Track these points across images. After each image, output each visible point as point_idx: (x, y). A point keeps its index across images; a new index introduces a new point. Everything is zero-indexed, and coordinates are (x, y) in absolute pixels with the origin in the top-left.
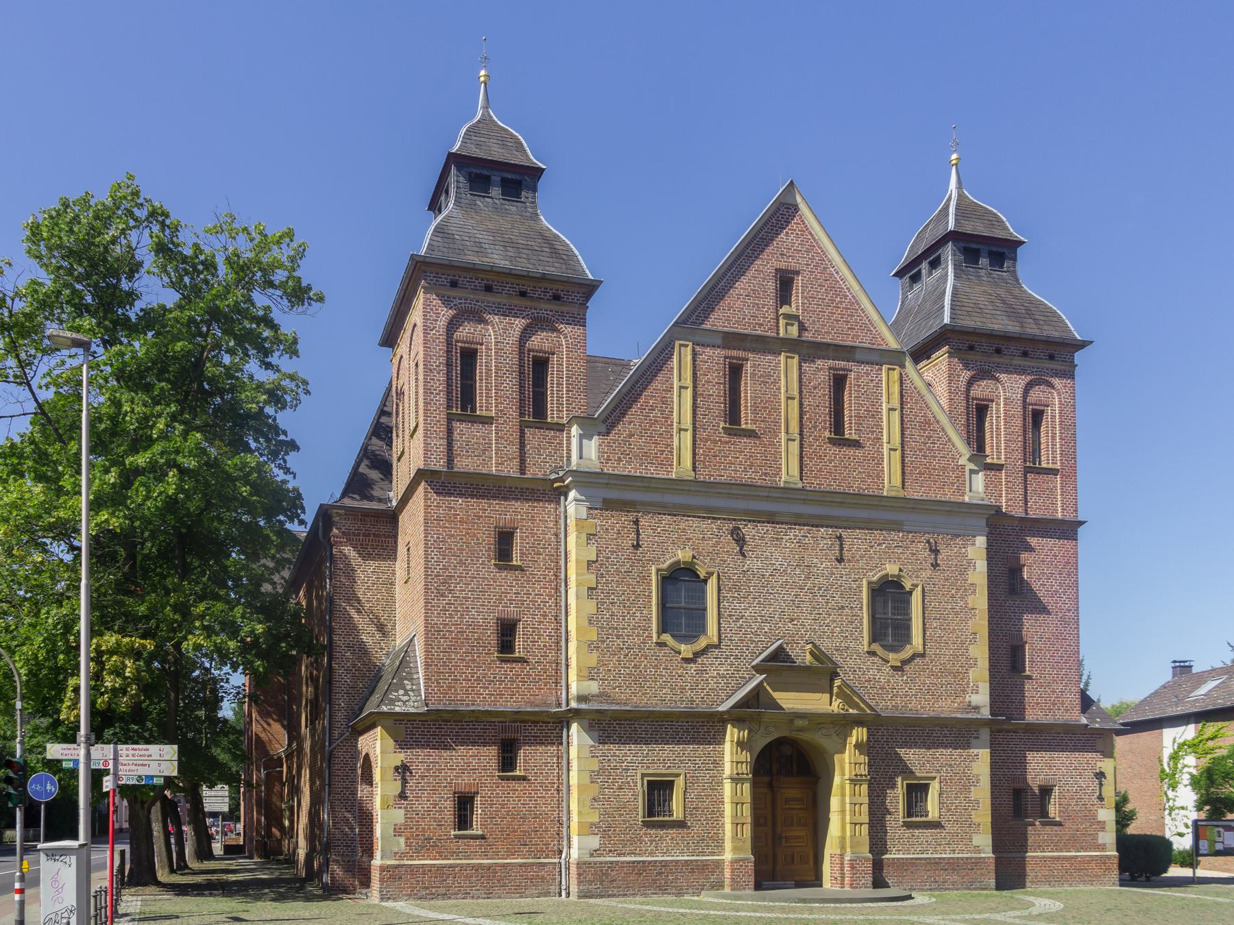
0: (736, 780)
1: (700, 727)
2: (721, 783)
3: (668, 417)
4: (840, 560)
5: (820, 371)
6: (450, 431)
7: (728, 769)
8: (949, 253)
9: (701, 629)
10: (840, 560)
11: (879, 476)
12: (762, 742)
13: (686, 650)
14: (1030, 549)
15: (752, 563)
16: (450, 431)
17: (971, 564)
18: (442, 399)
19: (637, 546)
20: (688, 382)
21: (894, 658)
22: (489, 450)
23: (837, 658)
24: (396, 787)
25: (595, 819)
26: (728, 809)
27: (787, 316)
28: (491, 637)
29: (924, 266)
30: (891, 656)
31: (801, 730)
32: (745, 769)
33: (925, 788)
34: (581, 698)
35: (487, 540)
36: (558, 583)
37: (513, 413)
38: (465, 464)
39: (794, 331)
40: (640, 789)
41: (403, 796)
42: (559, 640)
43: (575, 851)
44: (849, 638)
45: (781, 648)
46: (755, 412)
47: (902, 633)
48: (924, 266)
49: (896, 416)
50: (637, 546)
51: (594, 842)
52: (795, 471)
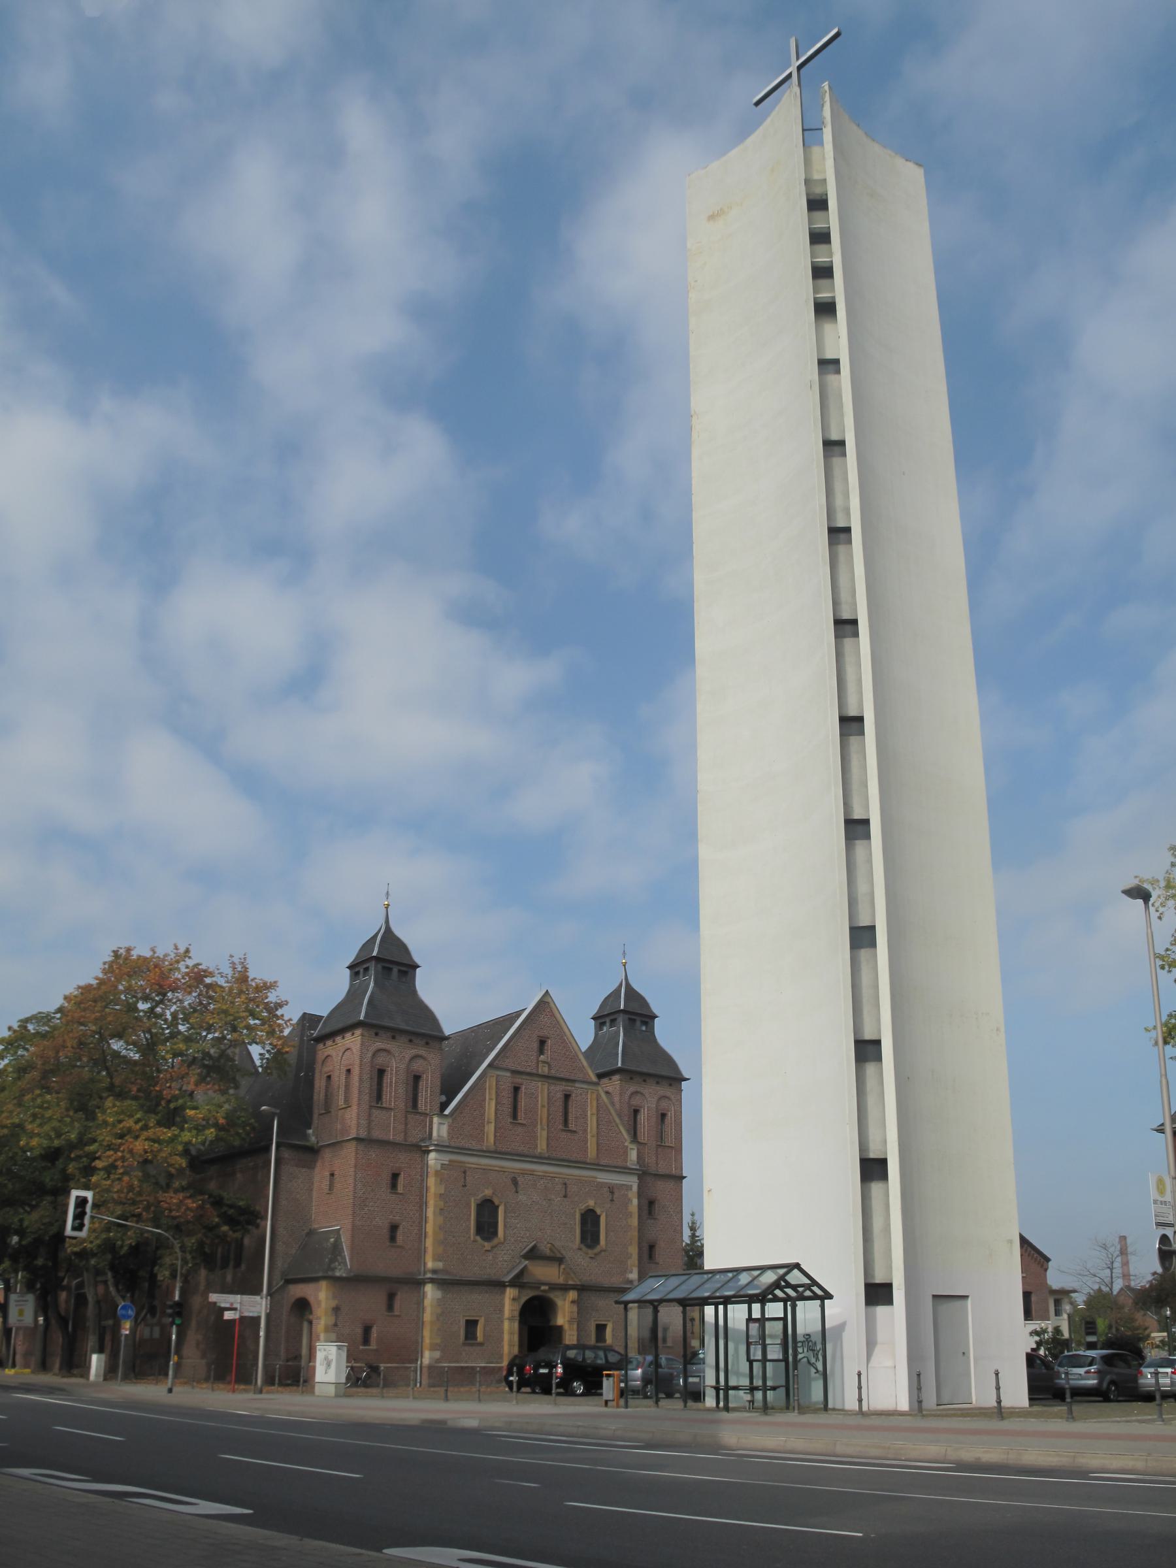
0: (511, 1319)
1: (500, 1285)
2: (502, 1322)
3: (483, 1115)
4: (565, 1196)
5: (559, 1090)
6: (370, 1115)
7: (507, 1313)
8: (621, 1020)
9: (495, 1233)
10: (565, 1196)
11: (586, 1151)
12: (524, 1300)
13: (487, 1246)
14: (97, 978)
15: (522, 1197)
16: (370, 1115)
17: (630, 1200)
18: (367, 1098)
19: (464, 1186)
20: (494, 1096)
21: (591, 1252)
22: (391, 1127)
23: (564, 1252)
24: (332, 1320)
25: (438, 1341)
26: (506, 1337)
27: (544, 1062)
28: (385, 1232)
29: (608, 1020)
30: (590, 1251)
31: (544, 1291)
32: (517, 1313)
33: (605, 1326)
34: (434, 1271)
35: (386, 1177)
36: (422, 1205)
37: (402, 1105)
38: (377, 1134)
39: (546, 1069)
40: (463, 1323)
41: (336, 1325)
42: (421, 1235)
43: (427, 1357)
44: (569, 1240)
45: (534, 1247)
46: (526, 1114)
47: (596, 1240)
48: (608, 1020)
49: (595, 1118)
50: (464, 1186)
51: (437, 1354)
52: (545, 1147)
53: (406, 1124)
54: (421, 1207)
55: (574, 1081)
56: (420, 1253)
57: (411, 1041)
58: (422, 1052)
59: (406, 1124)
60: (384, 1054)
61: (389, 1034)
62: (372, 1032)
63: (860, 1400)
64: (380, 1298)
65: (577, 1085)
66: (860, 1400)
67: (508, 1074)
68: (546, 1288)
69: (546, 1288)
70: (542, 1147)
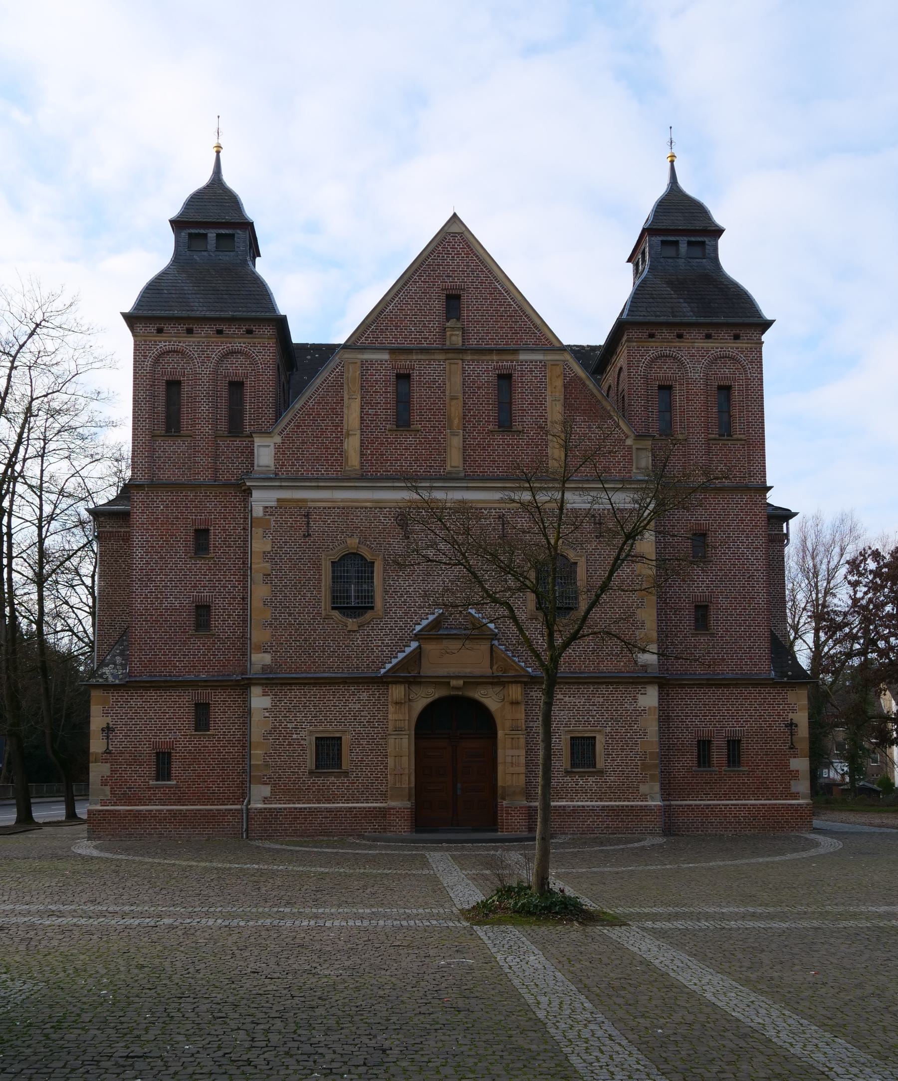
14: (452, 279)
53: (216, 457)
54: (245, 575)
55: (515, 351)
56: (243, 647)
57: (220, 332)
58: (239, 344)
59: (216, 457)
60: (176, 357)
61: (181, 328)
62: (152, 329)
63: (804, 641)
64: (181, 704)
65: (522, 357)
66: (804, 641)
67: (386, 356)
68: (460, 682)
69: (461, 682)
70: (455, 460)
